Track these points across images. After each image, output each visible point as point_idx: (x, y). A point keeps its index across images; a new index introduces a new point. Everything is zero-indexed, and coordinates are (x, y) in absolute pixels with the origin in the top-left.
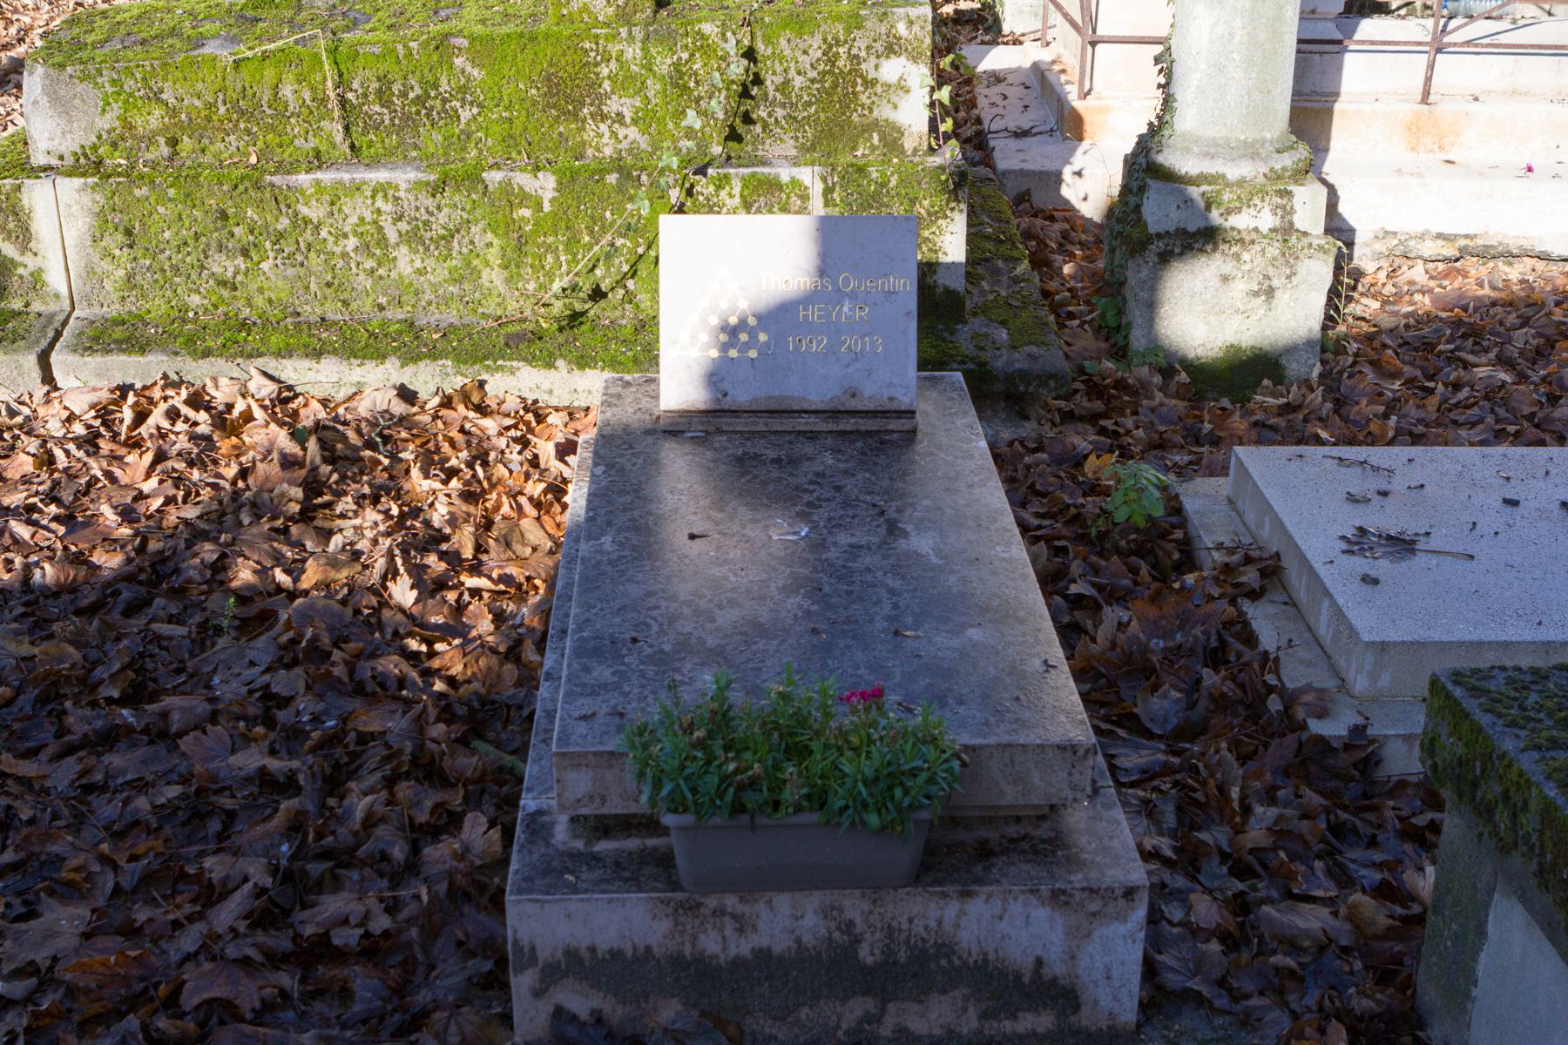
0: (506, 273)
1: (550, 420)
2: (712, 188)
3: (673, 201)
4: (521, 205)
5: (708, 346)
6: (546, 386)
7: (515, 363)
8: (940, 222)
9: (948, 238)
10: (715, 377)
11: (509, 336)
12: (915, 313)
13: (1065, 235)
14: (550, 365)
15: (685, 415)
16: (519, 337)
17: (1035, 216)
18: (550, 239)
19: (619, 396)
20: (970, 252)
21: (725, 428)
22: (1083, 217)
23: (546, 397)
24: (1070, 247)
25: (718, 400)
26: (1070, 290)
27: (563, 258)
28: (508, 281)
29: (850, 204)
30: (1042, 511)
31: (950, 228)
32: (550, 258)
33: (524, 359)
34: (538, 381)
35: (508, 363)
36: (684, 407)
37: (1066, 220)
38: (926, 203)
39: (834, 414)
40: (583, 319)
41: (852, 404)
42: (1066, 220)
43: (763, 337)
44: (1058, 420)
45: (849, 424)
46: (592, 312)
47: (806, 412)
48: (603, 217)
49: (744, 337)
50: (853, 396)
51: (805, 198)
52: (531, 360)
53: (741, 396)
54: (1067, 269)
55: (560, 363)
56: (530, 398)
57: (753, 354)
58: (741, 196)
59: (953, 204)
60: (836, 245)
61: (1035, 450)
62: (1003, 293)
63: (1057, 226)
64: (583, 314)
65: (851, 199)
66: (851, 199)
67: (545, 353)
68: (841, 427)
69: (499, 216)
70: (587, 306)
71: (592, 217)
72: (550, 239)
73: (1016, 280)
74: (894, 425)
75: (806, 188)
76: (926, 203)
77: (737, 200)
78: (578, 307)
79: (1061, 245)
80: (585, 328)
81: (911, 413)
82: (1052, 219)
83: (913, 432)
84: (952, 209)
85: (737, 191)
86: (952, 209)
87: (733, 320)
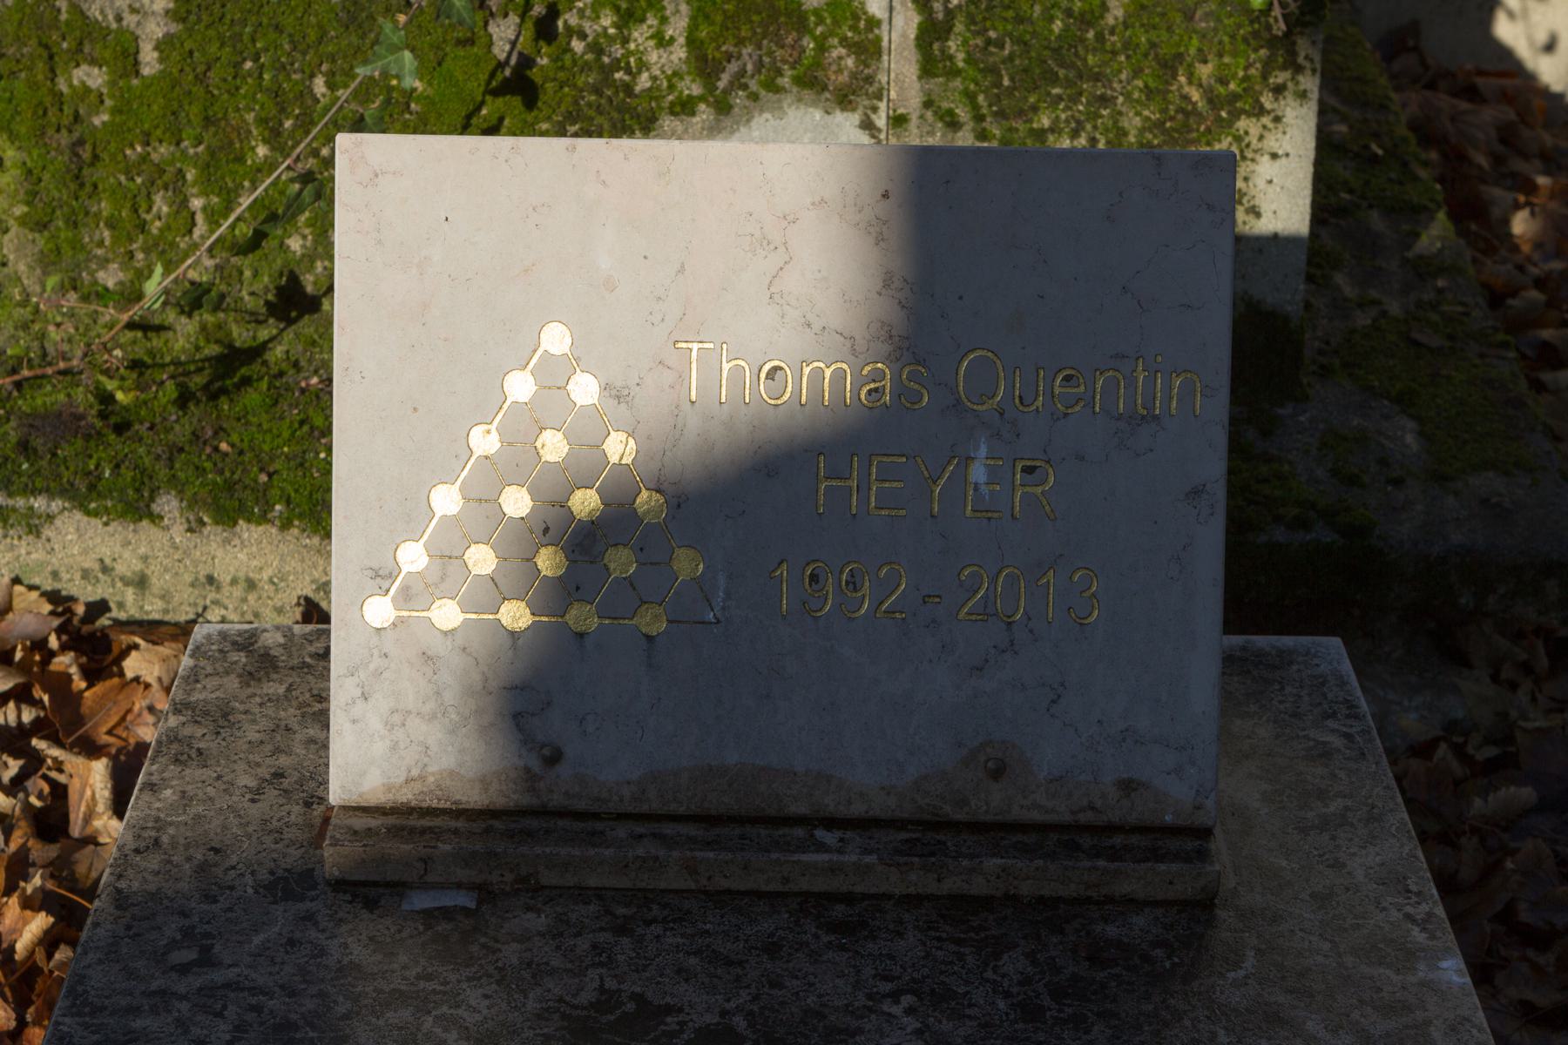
0: (41, 241)
1: (133, 665)
2: (607, 20)
3: (500, 50)
4: (77, 56)
5: (497, 589)
6: (128, 564)
7: (39, 503)
8: (1242, 124)
9: (1264, 169)
10: (531, 697)
11: (35, 422)
12: (1220, 493)
13: (1507, 135)
14: (138, 509)
15: (405, 822)
16: (65, 423)
17: (1431, 86)
18: (162, 151)
19: (222, 717)
20: (1322, 211)
21: (549, 878)
22: (1545, 93)
23: (130, 594)
24: (1519, 165)
25: (529, 778)
26: (1540, 283)
27: (197, 203)
28: (47, 262)
29: (993, 71)
30: (1545, 998)
31: (1271, 143)
32: (161, 204)
33: (67, 492)
34: (105, 552)
35: (20, 502)
36: (406, 796)
37: (1506, 97)
38: (1205, 71)
39: (926, 831)
40: (255, 368)
41: (993, 801)
42: (1506, 97)
43: (687, 565)
44: (1543, 662)
45: (986, 873)
46: (279, 351)
47: (831, 823)
48: (306, 93)
49: (621, 562)
50: (997, 773)
51: (868, 49)
52: (86, 494)
53: (610, 765)
54: (1520, 224)
55: (168, 504)
56: (85, 593)
57: (652, 621)
58: (691, 42)
59: (1280, 77)
60: (953, 237)
61: (1492, 767)
62: (1394, 308)
63: (1489, 115)
64: (256, 352)
65: (997, 55)
66: (997, 55)
67: (128, 474)
68: (951, 885)
69: (20, 85)
70: (264, 334)
71: (276, 93)
72: (162, 151)
73: (1424, 269)
74: (1135, 880)
75: (873, 23)
76: (1205, 71)
77: (679, 53)
78: (241, 335)
79: (1498, 160)
80: (252, 398)
81: (1189, 839)
82: (1471, 93)
83: (1202, 907)
84: (1278, 90)
85: (677, 27)
86: (1278, 90)
87: (585, 502)
